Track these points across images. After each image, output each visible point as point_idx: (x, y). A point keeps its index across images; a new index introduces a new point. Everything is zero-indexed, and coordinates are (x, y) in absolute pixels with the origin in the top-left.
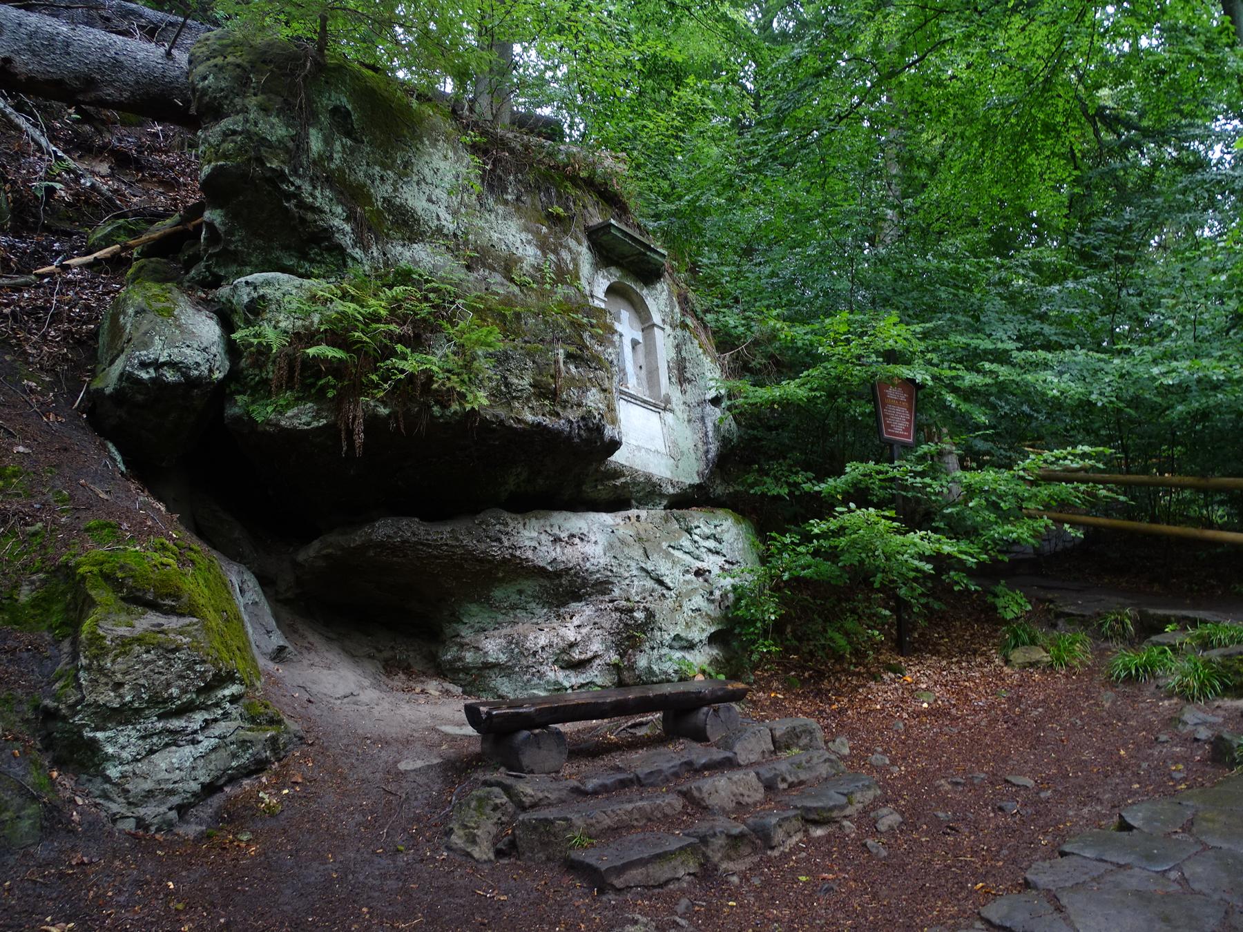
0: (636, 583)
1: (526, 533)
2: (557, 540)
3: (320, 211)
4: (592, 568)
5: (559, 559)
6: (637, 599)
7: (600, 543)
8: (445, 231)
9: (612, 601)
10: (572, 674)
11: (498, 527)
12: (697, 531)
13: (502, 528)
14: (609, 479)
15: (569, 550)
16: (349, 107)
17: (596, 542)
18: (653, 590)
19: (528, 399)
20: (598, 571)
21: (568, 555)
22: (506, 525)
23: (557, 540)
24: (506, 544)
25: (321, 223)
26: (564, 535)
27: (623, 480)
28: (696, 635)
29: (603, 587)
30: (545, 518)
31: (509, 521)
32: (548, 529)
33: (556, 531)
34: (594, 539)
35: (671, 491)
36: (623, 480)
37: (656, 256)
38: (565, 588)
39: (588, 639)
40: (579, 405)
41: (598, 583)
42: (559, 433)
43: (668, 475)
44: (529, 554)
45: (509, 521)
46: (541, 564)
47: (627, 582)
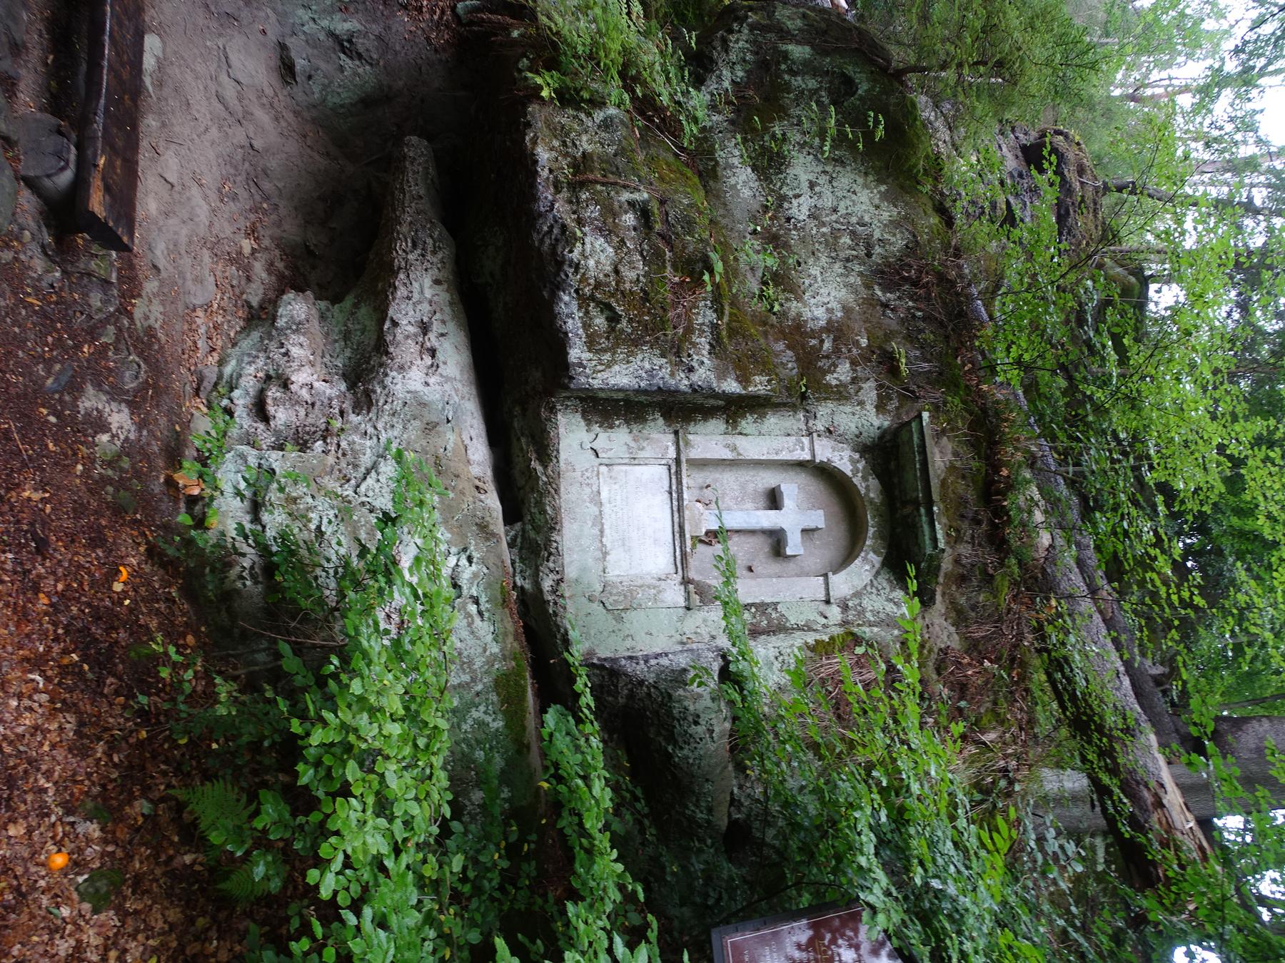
0: (368, 443)
1: (427, 282)
2: (425, 328)
3: (726, 49)
4: (388, 381)
5: (399, 330)
6: (344, 444)
7: (426, 389)
8: (786, 205)
9: (342, 413)
10: (248, 401)
11: (429, 241)
12: (464, 562)
13: (430, 247)
14: (537, 452)
15: (414, 348)
16: (860, 92)
17: (427, 384)
18: (356, 466)
19: (566, 155)
20: (384, 388)
21: (405, 347)
22: (434, 253)
23: (425, 328)
24: (410, 257)
25: (715, 54)
26: (432, 339)
27: (539, 469)
28: (274, 520)
29: (364, 402)
30: (455, 317)
31: (440, 255)
32: (438, 316)
33: (436, 327)
34: (432, 380)
35: (547, 584)
36: (539, 469)
37: (926, 528)
38: (363, 372)
39: (296, 402)
40: (580, 222)
41: (368, 394)
42: (535, 198)
43: (571, 572)
44: (402, 292)
45: (440, 255)
46: (391, 313)
47: (370, 430)
